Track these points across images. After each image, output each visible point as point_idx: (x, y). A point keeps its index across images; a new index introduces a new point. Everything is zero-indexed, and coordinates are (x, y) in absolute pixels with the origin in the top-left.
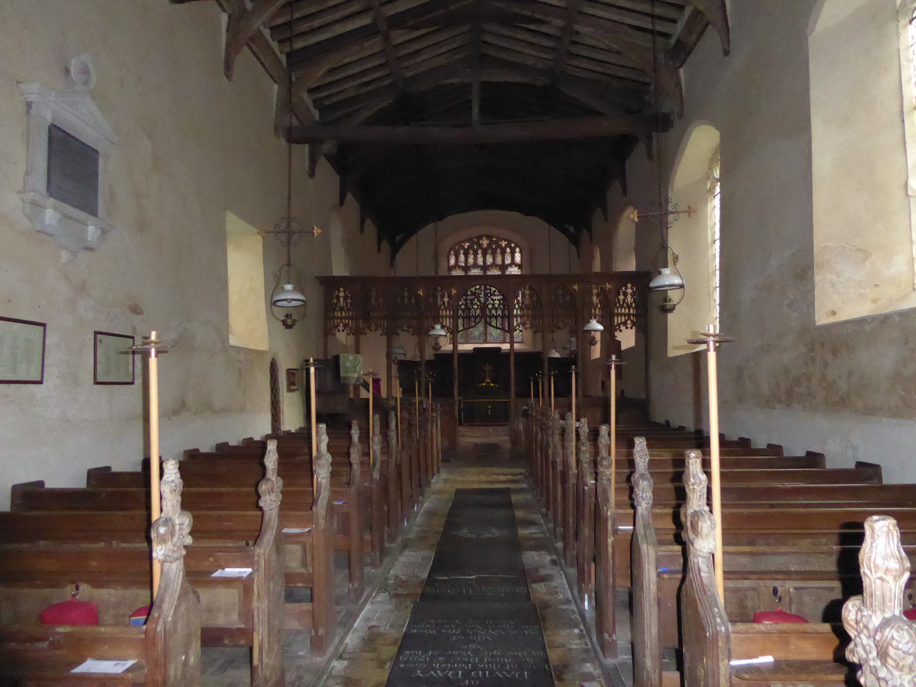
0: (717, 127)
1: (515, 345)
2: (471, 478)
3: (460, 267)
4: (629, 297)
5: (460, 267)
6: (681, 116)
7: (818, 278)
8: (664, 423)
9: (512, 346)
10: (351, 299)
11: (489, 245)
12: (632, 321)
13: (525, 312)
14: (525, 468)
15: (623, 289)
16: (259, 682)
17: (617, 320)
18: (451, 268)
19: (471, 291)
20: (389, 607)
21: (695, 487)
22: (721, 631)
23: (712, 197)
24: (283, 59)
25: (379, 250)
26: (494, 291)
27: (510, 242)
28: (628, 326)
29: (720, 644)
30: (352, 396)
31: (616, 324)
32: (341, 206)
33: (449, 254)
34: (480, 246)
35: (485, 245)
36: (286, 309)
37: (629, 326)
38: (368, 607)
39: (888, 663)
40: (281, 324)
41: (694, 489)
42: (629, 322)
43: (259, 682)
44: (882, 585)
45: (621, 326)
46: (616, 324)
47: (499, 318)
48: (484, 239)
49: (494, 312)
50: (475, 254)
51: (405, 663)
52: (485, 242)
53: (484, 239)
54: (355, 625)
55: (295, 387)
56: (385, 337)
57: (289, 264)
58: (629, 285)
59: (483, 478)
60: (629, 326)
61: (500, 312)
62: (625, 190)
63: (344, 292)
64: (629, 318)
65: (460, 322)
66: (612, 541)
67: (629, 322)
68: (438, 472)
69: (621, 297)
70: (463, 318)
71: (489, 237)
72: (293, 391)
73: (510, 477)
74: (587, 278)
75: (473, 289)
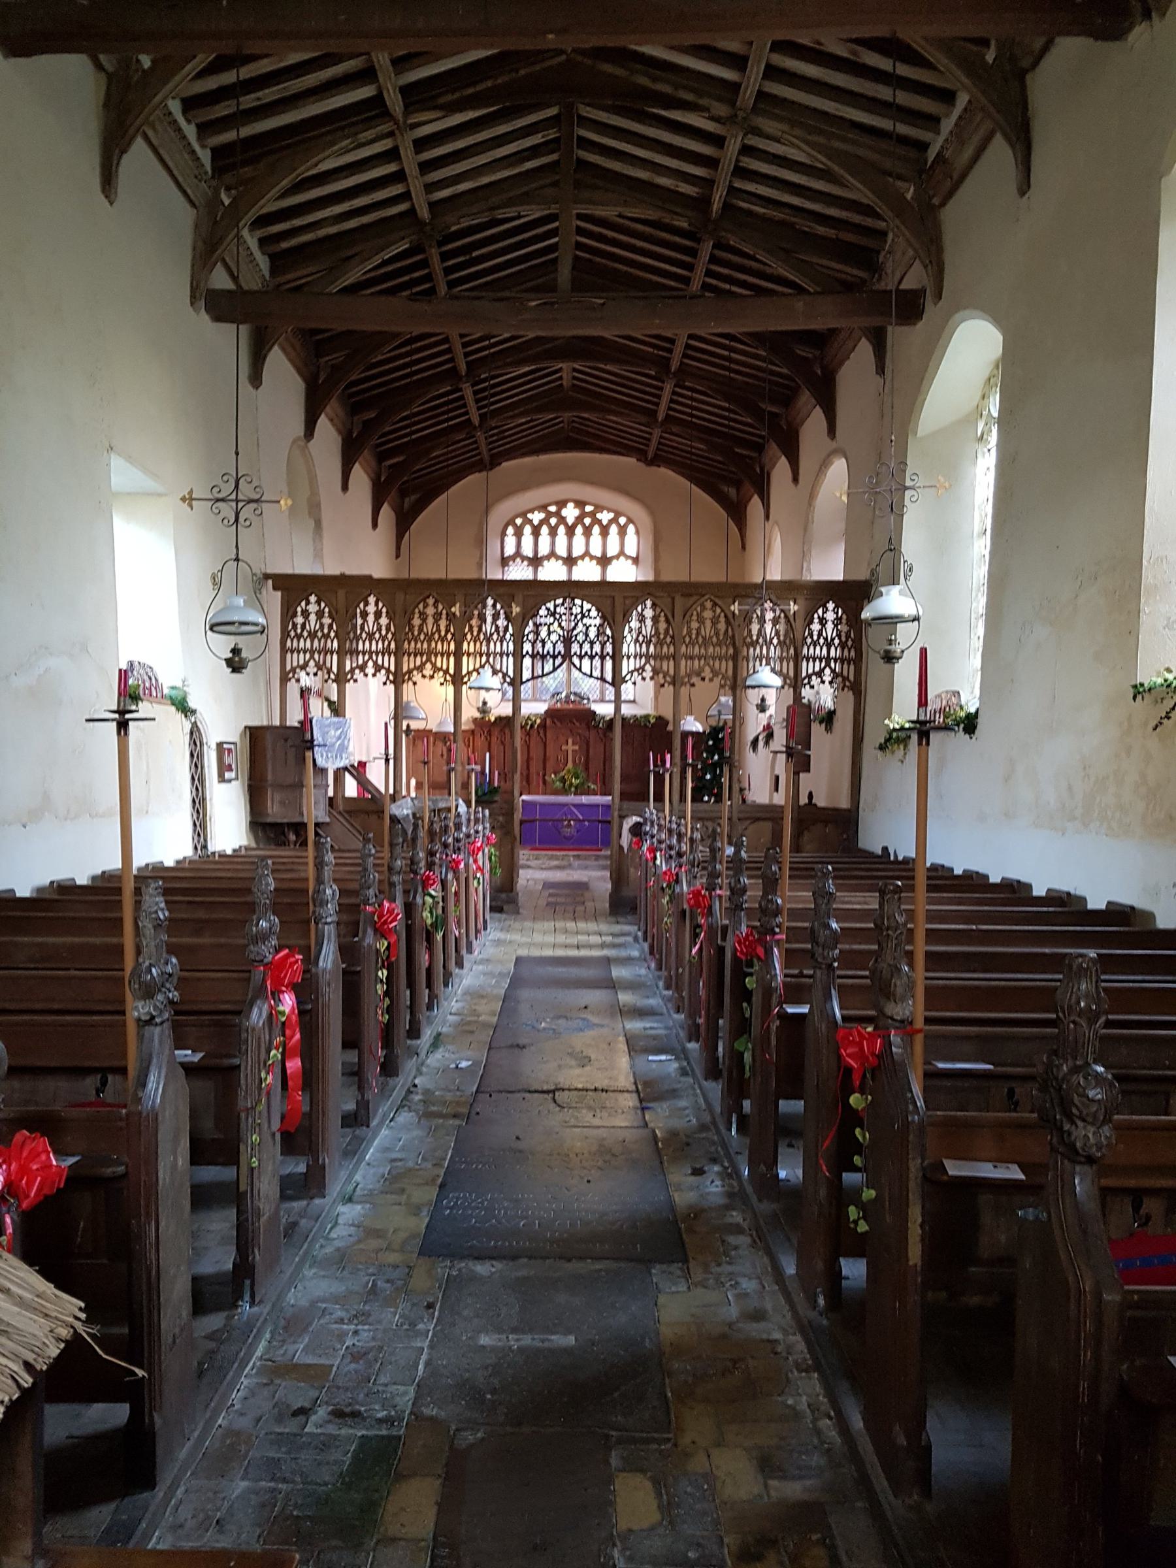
0: (997, 321)
1: (623, 706)
2: (538, 938)
3: (524, 558)
4: (830, 626)
5: (524, 558)
6: (939, 296)
7: (1146, 609)
8: (880, 852)
9: (618, 709)
10: (330, 616)
11: (579, 520)
12: (833, 671)
13: (644, 649)
14: (635, 924)
15: (820, 611)
16: (823, 682)
17: (807, 668)
18: (505, 561)
19: (548, 609)
20: (417, 1133)
21: (890, 932)
22: (913, 1121)
23: (986, 450)
24: (205, 156)
25: (375, 525)
26: (589, 611)
27: (618, 514)
28: (824, 678)
29: (911, 1138)
30: (331, 793)
31: (804, 674)
32: (309, 441)
33: (503, 534)
34: (562, 520)
35: (570, 521)
36: (232, 637)
37: (827, 678)
38: (384, 1132)
39: (752, 823)
40: (224, 663)
41: (888, 935)
42: (827, 671)
43: (823, 682)
44: (1075, 1028)
45: (814, 677)
46: (804, 674)
47: (597, 657)
48: (571, 505)
49: (586, 647)
50: (553, 532)
51: (451, 1208)
52: (570, 513)
53: (571, 505)
54: (367, 1157)
55: (233, 775)
56: (391, 688)
57: (237, 559)
58: (831, 606)
59: (561, 938)
60: (827, 678)
61: (597, 648)
62: (832, 431)
63: (318, 603)
64: (828, 665)
65: (527, 662)
66: (777, 1027)
67: (827, 671)
68: (485, 928)
69: (816, 627)
70: (533, 657)
71: (580, 504)
72: (230, 781)
73: (609, 939)
74: (752, 593)
75: (551, 605)
